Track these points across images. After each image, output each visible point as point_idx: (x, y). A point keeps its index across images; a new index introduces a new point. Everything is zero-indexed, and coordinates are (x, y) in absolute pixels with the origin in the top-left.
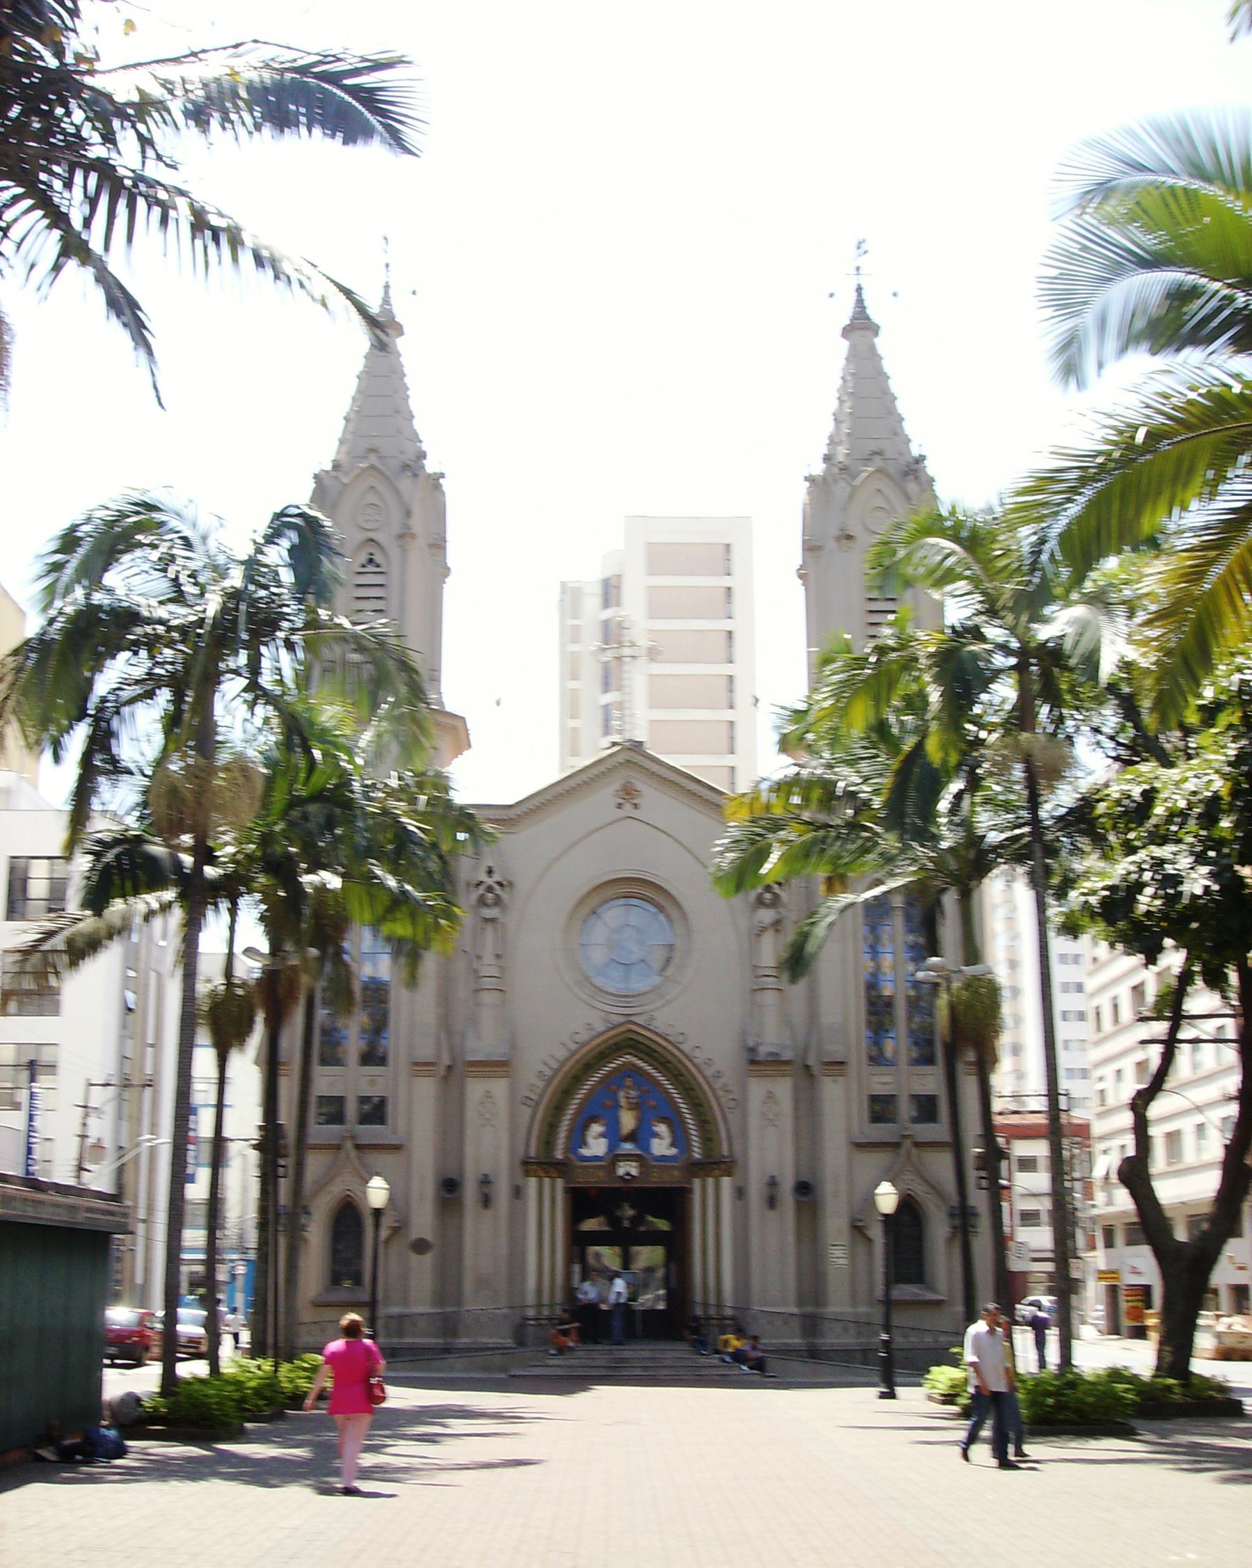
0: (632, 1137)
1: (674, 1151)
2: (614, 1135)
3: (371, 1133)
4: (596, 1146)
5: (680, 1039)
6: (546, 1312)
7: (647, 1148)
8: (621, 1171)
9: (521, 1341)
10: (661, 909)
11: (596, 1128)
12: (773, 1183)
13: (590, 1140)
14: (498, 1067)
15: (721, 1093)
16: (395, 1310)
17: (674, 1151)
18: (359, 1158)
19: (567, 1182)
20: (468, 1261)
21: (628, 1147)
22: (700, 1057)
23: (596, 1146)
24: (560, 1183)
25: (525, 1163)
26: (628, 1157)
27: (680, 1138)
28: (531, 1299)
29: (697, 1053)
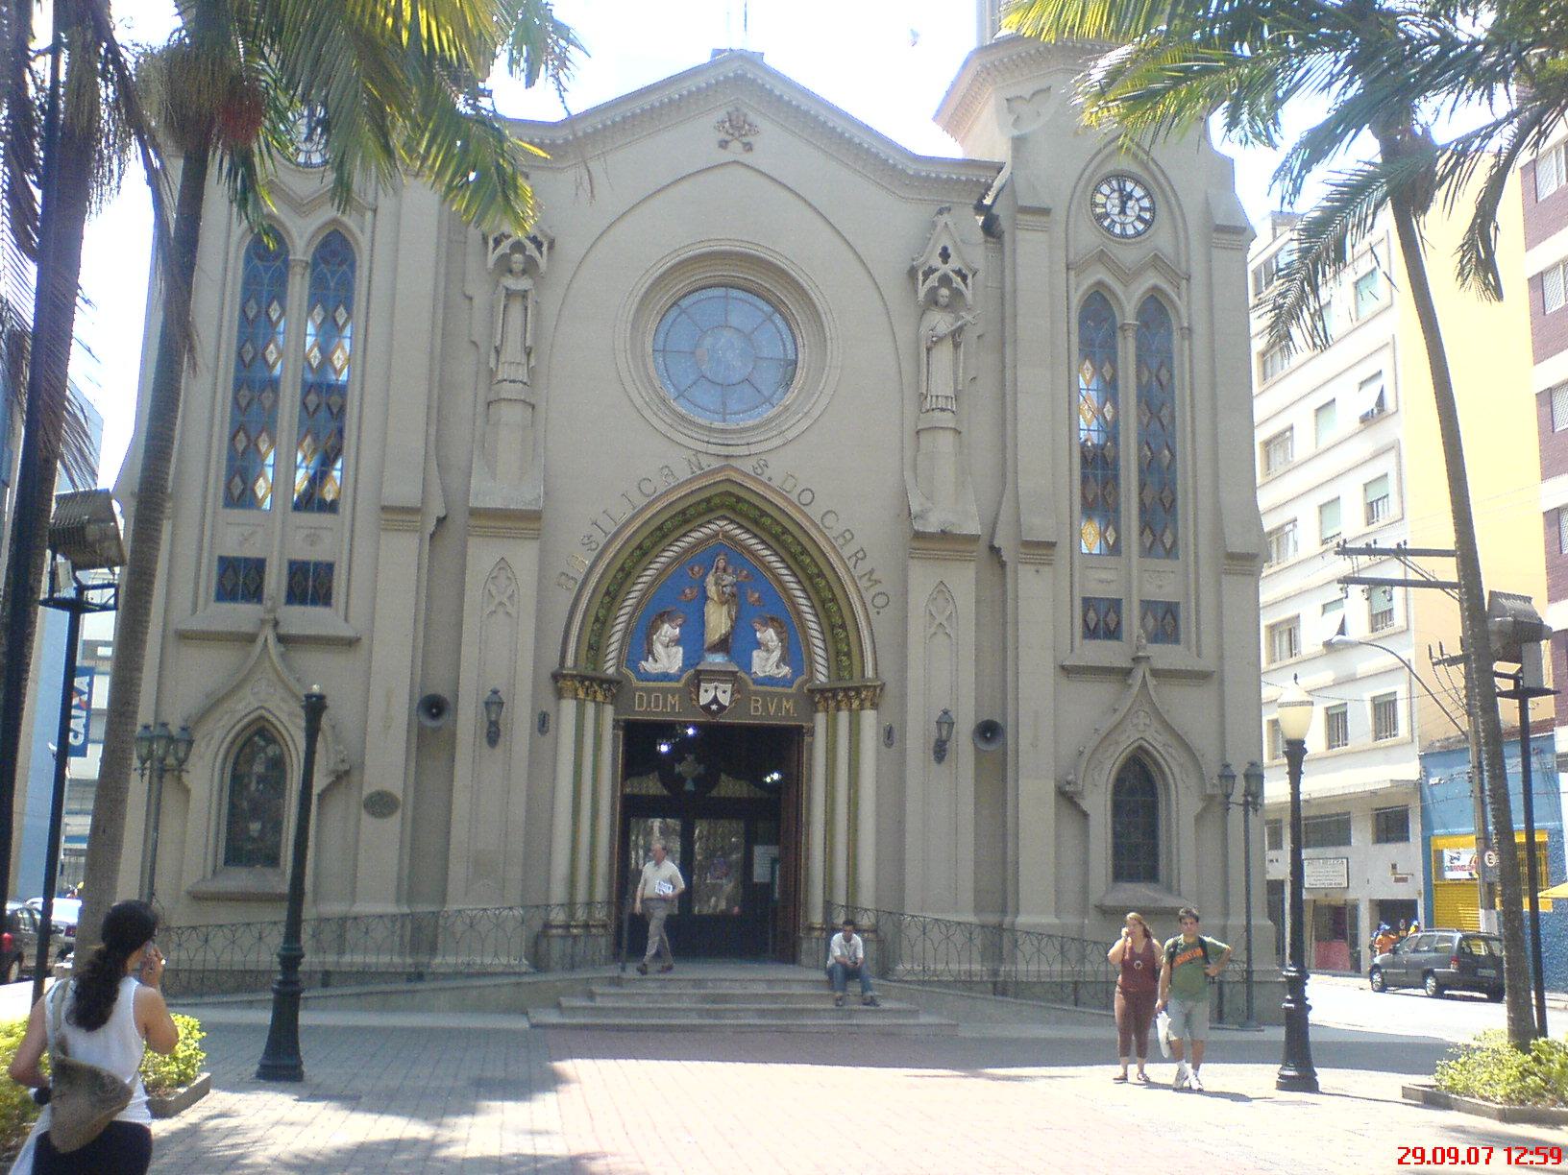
0: (723, 645)
1: (785, 670)
2: (693, 641)
3: (302, 619)
4: (667, 657)
5: (806, 497)
6: (581, 915)
7: (747, 666)
8: (705, 699)
9: (539, 961)
10: (777, 306)
11: (668, 631)
12: (946, 721)
13: (658, 648)
14: (523, 522)
15: (863, 583)
16: (334, 908)
17: (785, 670)
18: (283, 656)
19: (617, 712)
20: (459, 832)
21: (717, 660)
22: (835, 527)
23: (667, 657)
24: (609, 711)
25: (556, 677)
26: (716, 675)
27: (794, 652)
28: (558, 893)
29: (830, 520)
